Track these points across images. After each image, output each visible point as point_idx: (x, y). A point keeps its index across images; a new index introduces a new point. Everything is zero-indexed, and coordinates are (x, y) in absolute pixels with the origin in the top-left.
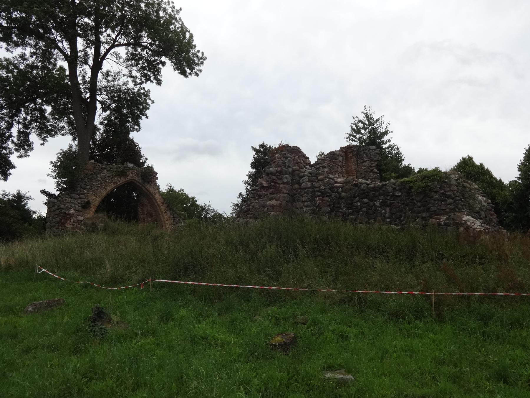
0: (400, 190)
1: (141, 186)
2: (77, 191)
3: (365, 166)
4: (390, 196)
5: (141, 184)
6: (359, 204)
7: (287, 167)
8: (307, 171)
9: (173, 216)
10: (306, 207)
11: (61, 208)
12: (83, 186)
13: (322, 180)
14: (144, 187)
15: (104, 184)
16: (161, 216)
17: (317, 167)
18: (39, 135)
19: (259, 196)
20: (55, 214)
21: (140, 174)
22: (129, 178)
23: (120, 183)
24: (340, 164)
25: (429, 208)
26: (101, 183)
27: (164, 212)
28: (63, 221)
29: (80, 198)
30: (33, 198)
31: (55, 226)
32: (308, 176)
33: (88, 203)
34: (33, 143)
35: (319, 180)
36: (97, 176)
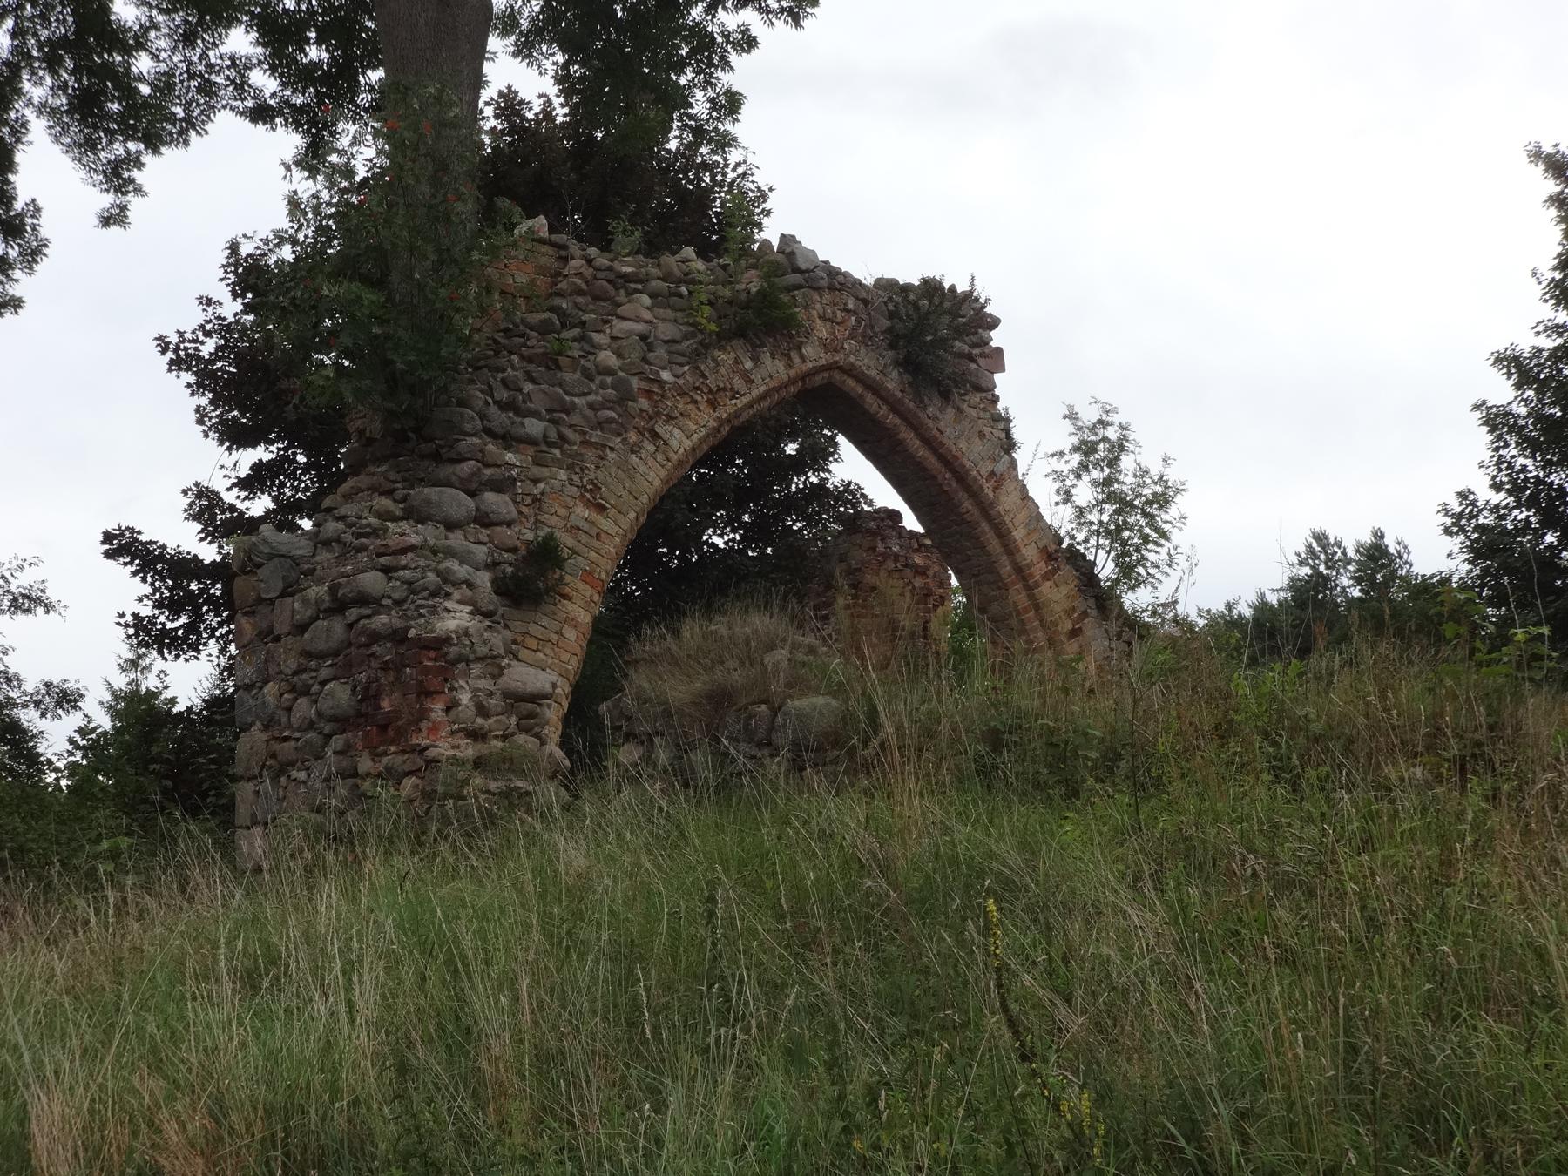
1: (892, 419)
2: (463, 460)
5: (895, 407)
11: (363, 600)
12: (499, 418)
14: (917, 428)
15: (644, 403)
18: (86, 147)
20: (307, 654)
21: (886, 323)
22: (814, 354)
23: (755, 393)
26: (625, 396)
27: (1069, 626)
28: (386, 705)
29: (484, 520)
30: (54, 599)
31: (319, 757)
33: (546, 555)
34: (38, 210)
36: (582, 339)
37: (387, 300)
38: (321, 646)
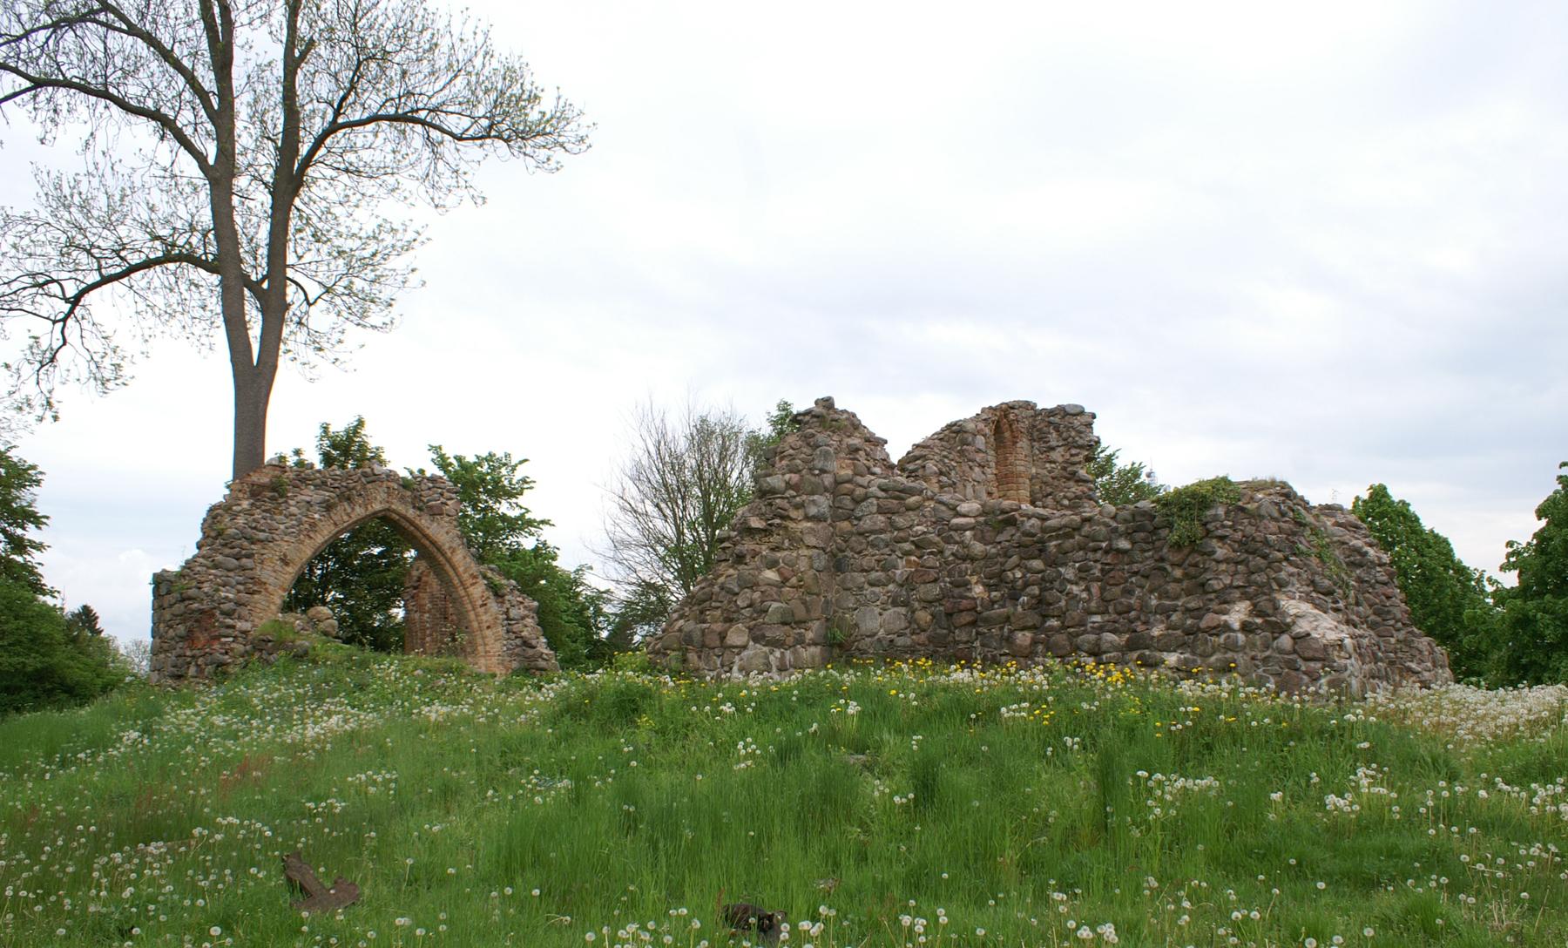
0: (1128, 535)
3: (1054, 462)
4: (1100, 552)
6: (1019, 575)
7: (817, 472)
8: (874, 484)
9: (505, 616)
10: (872, 584)
11: (190, 598)
13: (918, 508)
16: (472, 615)
17: (911, 467)
19: (738, 556)
24: (978, 459)
25: (1203, 585)
27: (480, 602)
29: (244, 569)
32: (878, 498)
35: (909, 509)
36: (286, 502)
37: (1128, 499)
38: (177, 613)
